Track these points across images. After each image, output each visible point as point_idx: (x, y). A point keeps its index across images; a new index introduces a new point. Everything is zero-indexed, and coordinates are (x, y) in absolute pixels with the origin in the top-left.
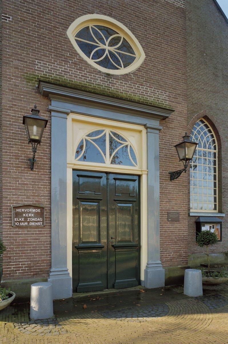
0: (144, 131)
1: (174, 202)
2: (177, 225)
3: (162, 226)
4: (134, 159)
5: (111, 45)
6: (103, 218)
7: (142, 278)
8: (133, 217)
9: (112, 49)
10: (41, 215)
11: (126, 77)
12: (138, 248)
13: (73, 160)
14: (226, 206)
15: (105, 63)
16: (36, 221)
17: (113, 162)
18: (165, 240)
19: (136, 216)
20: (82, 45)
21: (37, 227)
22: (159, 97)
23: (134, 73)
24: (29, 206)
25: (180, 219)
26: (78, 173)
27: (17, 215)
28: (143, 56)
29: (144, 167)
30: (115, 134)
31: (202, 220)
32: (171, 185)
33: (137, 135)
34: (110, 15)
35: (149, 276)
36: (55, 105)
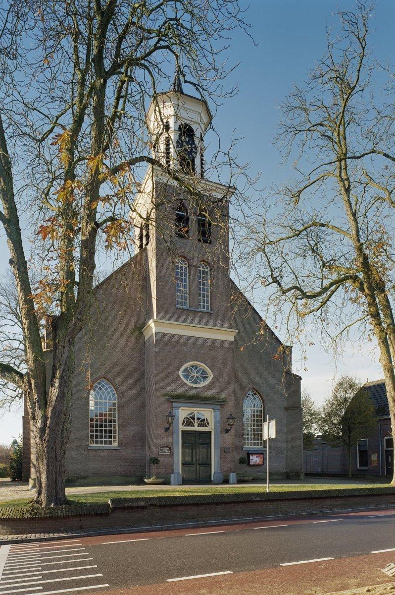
0: (213, 411)
1: (227, 443)
2: (229, 454)
3: (221, 455)
4: (193, 413)
5: (197, 373)
6: (194, 452)
7: (212, 479)
8: (208, 450)
9: (197, 375)
10: (170, 450)
11: (204, 387)
12: (211, 464)
13: (182, 428)
14: (390, 246)
15: (195, 382)
16: (168, 453)
17: (199, 425)
18: (222, 462)
19: (209, 450)
20: (184, 376)
21: (168, 455)
22: (220, 394)
23: (208, 385)
24: (165, 447)
25: (198, 450)
26: (183, 432)
27: (161, 450)
28: (212, 376)
29: (213, 427)
30: (198, 413)
31: (250, 452)
32: (226, 435)
33: (209, 413)
34: (197, 361)
35: (215, 477)
36: (175, 405)
